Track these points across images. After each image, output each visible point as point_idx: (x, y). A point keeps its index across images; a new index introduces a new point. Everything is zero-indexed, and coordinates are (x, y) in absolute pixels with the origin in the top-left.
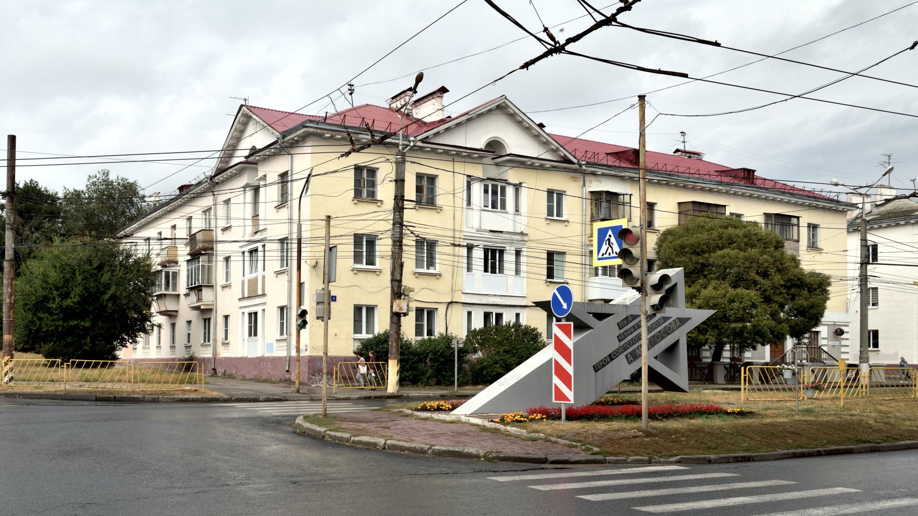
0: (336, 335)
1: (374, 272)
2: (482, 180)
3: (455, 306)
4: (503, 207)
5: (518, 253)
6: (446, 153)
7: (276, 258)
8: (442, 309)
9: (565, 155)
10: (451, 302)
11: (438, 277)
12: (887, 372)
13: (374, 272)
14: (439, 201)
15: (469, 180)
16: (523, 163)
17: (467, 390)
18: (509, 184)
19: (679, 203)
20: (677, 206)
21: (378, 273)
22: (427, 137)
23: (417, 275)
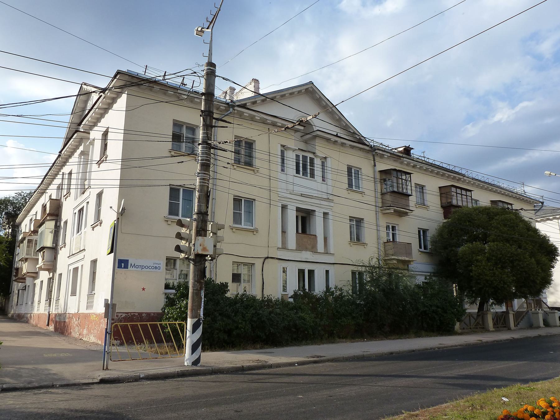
0: (144, 289)
1: (252, 231)
2: (294, 150)
3: (269, 259)
4: (312, 175)
5: (325, 214)
6: (264, 122)
7: (402, 233)
8: (258, 264)
9: (249, 114)
10: (268, 258)
11: (255, 233)
12: (157, 314)
13: (252, 231)
14: (257, 163)
15: (283, 149)
16: (328, 140)
17: (493, 323)
18: (317, 156)
19: (440, 187)
20: (438, 190)
21: (255, 233)
22: (246, 104)
23: (234, 230)
